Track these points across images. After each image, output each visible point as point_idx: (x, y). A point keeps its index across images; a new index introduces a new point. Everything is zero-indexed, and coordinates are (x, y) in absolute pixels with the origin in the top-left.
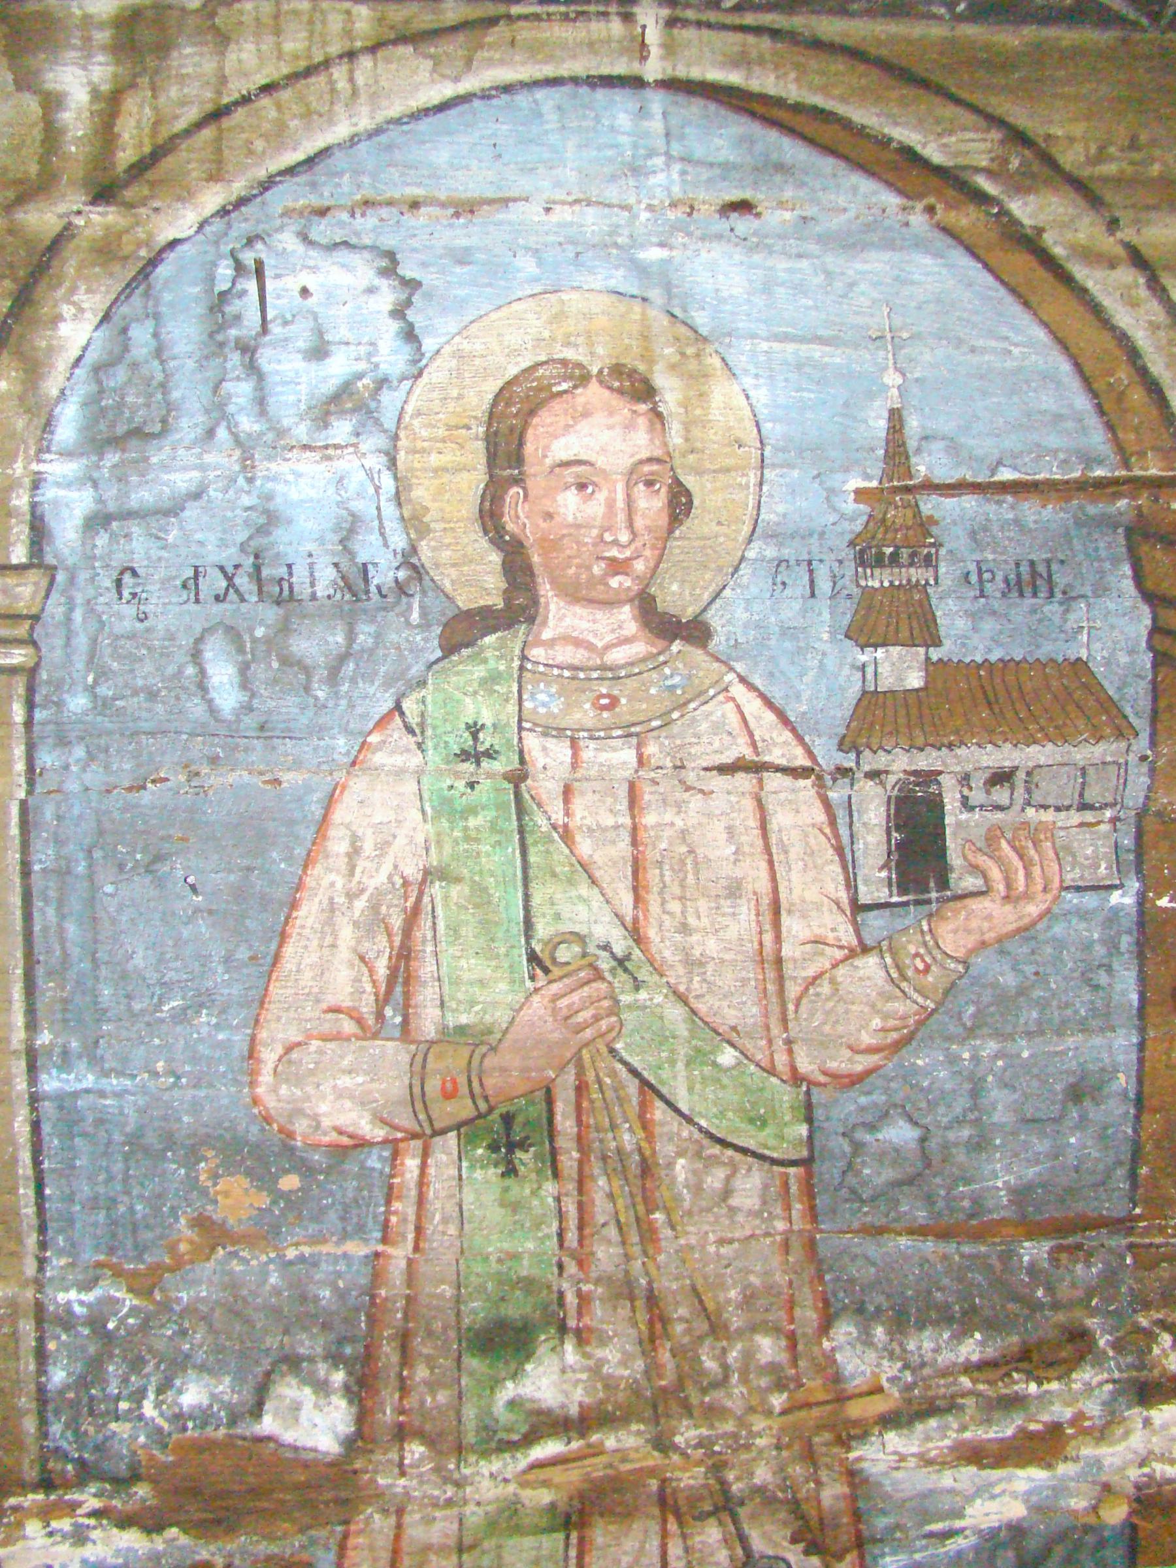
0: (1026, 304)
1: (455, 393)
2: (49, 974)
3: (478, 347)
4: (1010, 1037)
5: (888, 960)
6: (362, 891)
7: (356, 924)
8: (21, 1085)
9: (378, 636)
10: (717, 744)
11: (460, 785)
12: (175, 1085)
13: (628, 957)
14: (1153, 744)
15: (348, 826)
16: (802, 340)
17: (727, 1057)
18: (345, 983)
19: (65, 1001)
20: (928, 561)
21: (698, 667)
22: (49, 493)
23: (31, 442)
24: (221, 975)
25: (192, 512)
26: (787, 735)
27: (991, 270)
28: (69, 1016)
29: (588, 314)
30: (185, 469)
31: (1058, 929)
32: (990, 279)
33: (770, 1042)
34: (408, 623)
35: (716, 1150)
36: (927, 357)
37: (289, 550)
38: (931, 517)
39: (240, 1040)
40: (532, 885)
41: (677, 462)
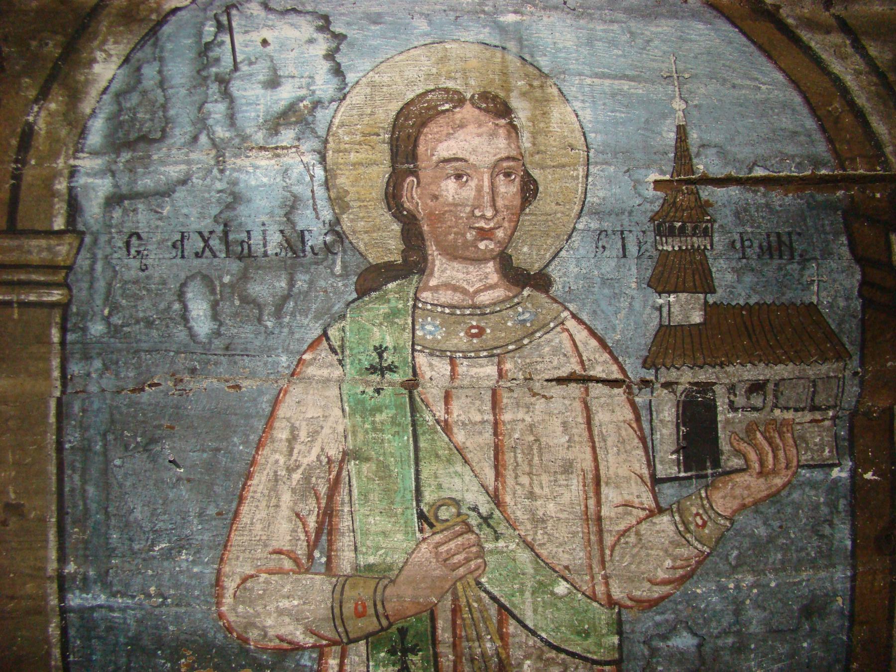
0: (770, 57)
1: (369, 111)
2: (75, 523)
3: (386, 79)
4: (763, 572)
5: (677, 518)
6: (298, 467)
7: (294, 491)
8: (54, 601)
9: (311, 283)
10: (555, 363)
11: (370, 391)
12: (163, 603)
13: (491, 516)
14: (862, 364)
15: (288, 420)
16: (615, 77)
17: (562, 588)
18: (284, 532)
19: (86, 542)
20: (706, 233)
21: (542, 307)
22: (82, 180)
23: (71, 145)
24: (196, 525)
25: (180, 193)
26: (606, 356)
27: (745, 34)
28: (88, 553)
29: (465, 56)
30: (176, 163)
31: (796, 495)
32: (744, 39)
33: (593, 578)
34: (333, 274)
35: (553, 654)
36: (703, 90)
37: (249, 221)
38: (707, 202)
39: (209, 572)
40: (422, 463)
41: (527, 159)
